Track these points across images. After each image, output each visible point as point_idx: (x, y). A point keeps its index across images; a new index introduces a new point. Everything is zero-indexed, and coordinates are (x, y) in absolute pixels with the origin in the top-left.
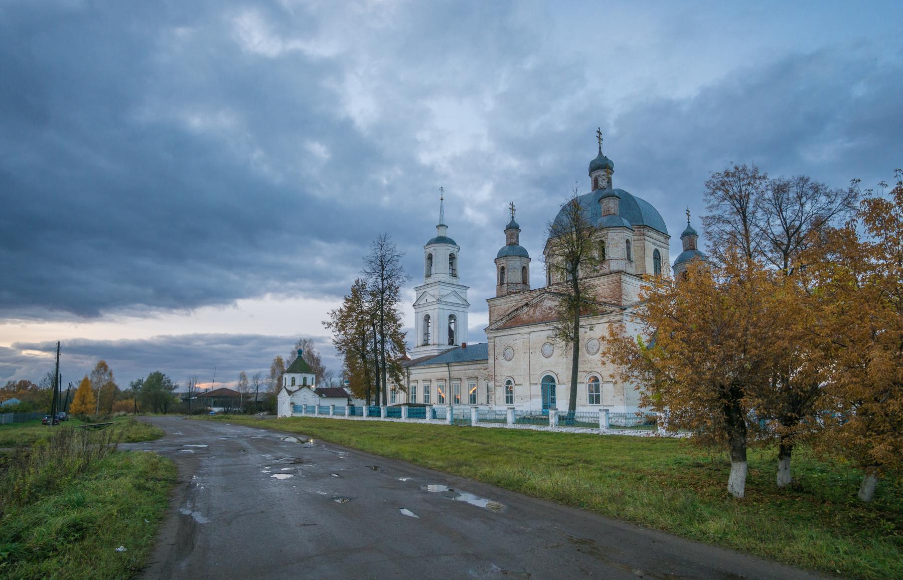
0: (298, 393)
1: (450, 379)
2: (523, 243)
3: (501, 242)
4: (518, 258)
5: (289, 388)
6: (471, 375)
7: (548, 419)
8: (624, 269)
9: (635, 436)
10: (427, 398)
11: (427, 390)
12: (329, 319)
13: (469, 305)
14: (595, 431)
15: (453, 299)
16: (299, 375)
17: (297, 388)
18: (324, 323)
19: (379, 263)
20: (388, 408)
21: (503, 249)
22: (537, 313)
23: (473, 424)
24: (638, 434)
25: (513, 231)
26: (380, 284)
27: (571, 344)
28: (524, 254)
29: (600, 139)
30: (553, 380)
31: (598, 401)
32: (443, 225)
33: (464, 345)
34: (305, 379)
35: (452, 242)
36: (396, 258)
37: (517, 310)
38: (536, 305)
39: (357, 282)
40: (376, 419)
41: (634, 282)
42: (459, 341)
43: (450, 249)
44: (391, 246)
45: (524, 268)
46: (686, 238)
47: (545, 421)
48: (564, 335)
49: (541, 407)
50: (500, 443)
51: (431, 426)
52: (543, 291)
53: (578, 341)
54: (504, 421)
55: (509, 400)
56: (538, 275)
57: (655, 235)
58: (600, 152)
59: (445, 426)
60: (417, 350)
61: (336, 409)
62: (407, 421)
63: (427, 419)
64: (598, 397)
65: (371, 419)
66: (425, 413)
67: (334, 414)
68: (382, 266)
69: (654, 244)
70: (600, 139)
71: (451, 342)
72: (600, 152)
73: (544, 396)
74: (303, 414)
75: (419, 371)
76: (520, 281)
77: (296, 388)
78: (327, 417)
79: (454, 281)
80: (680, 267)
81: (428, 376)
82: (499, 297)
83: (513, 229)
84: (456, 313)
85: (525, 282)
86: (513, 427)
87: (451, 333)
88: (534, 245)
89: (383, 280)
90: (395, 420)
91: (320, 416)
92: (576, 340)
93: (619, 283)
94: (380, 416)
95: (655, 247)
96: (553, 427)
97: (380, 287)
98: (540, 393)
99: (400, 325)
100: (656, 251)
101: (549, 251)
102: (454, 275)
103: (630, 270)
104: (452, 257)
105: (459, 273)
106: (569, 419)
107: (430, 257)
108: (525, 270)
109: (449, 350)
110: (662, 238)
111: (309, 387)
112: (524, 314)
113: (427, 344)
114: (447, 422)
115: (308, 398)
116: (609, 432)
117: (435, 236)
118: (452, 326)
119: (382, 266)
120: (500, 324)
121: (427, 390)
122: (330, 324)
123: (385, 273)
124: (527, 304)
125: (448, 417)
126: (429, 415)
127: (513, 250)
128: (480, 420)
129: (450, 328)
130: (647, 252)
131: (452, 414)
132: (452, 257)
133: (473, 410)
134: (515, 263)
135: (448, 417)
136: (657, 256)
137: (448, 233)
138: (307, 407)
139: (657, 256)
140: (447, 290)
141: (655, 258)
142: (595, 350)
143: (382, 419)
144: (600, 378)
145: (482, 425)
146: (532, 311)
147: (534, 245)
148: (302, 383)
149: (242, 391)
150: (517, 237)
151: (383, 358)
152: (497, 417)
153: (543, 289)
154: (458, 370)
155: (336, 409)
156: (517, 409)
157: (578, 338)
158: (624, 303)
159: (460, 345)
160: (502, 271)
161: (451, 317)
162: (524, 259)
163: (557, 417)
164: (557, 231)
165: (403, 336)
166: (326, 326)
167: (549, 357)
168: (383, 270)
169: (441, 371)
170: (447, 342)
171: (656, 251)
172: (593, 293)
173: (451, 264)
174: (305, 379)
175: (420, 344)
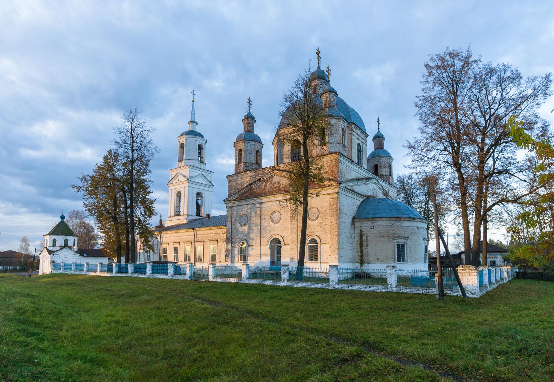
0: (58, 253)
1: (195, 241)
2: (257, 131)
3: (241, 129)
4: (253, 143)
5: (51, 249)
6: (212, 238)
7: (280, 274)
8: (340, 151)
9: (364, 291)
10: (176, 257)
11: (176, 250)
12: (79, 183)
13: (213, 186)
14: (325, 286)
15: (200, 180)
16: (60, 237)
17: (58, 248)
18: (73, 187)
19: (129, 134)
20: (216, 270)
21: (241, 134)
22: (268, 187)
23: (210, 279)
24: (368, 289)
25: (250, 120)
26: (130, 154)
27: (301, 207)
28: (257, 140)
29: (319, 57)
30: (279, 242)
31: (316, 259)
32: (194, 122)
33: (208, 216)
34: (66, 241)
35: (201, 136)
36: (146, 132)
37: (252, 184)
38: (266, 181)
39: (110, 153)
40: (124, 275)
41: (347, 163)
42: (204, 213)
43: (199, 141)
44: (141, 121)
45: (258, 151)
46: (377, 140)
47: (277, 275)
48: (296, 201)
49: (269, 264)
50: (236, 303)
51: (172, 281)
52: (273, 168)
53: (307, 205)
54: (239, 276)
55: (244, 259)
56: (268, 160)
57: (359, 133)
58: (319, 67)
59: (184, 280)
60: (171, 219)
61: (97, 267)
62: (151, 276)
63: (169, 275)
64: (316, 256)
65: (119, 275)
66: (167, 269)
67: (101, 271)
68: (132, 137)
69: (358, 139)
70: (319, 57)
71: (198, 213)
72: (319, 67)
73: (272, 255)
74: (61, 271)
75: (169, 235)
76: (255, 161)
77: (57, 248)
78: (82, 273)
79: (202, 166)
80: (372, 160)
81: (177, 239)
82: (237, 173)
83: (249, 120)
84: (202, 191)
85: (258, 163)
86: (247, 282)
87: (198, 207)
88: (266, 133)
89: (133, 151)
90: (140, 276)
91: (76, 273)
92: (305, 204)
93: (338, 162)
94: (127, 272)
95: (358, 142)
96: (285, 280)
97: (131, 158)
98: (269, 252)
99: (149, 193)
100: (359, 144)
101: (279, 141)
102: (201, 162)
103: (344, 153)
104: (200, 148)
105: (206, 160)
106: (298, 274)
107: (182, 146)
108: (258, 153)
109: (196, 220)
110: (363, 136)
111: (70, 248)
112: (256, 188)
113: (179, 215)
114: (187, 277)
115: (69, 257)
116: (339, 287)
117: (187, 129)
118: (199, 202)
119: (132, 137)
120: (236, 196)
121: (176, 250)
122: (79, 188)
123: (135, 144)
124: (260, 180)
125: (188, 272)
126: (171, 271)
127: (249, 137)
128: (217, 276)
129: (197, 203)
130: (353, 144)
131: (191, 270)
132: (200, 148)
133: (211, 266)
134: (253, 146)
135: (188, 272)
136: (359, 150)
137: (198, 129)
138: (65, 265)
139: (359, 150)
140: (196, 173)
141: (358, 150)
142: (315, 217)
143: (129, 275)
144: (318, 240)
145: (219, 280)
146: (263, 185)
147: (266, 133)
148: (63, 244)
149: (23, 252)
150: (253, 127)
151: (132, 221)
152: (233, 272)
153: (273, 167)
154: (202, 233)
155: (97, 267)
156: (251, 265)
157: (307, 202)
158: (340, 179)
159: (205, 216)
160: (239, 153)
161: (199, 194)
162: (257, 144)
163: (288, 273)
164: (287, 119)
165: (152, 202)
166: (75, 189)
167: (277, 223)
168: (133, 142)
169: (188, 234)
170: (194, 214)
171: (359, 144)
172: (320, 164)
173: (199, 153)
174: (66, 241)
175: (173, 215)
